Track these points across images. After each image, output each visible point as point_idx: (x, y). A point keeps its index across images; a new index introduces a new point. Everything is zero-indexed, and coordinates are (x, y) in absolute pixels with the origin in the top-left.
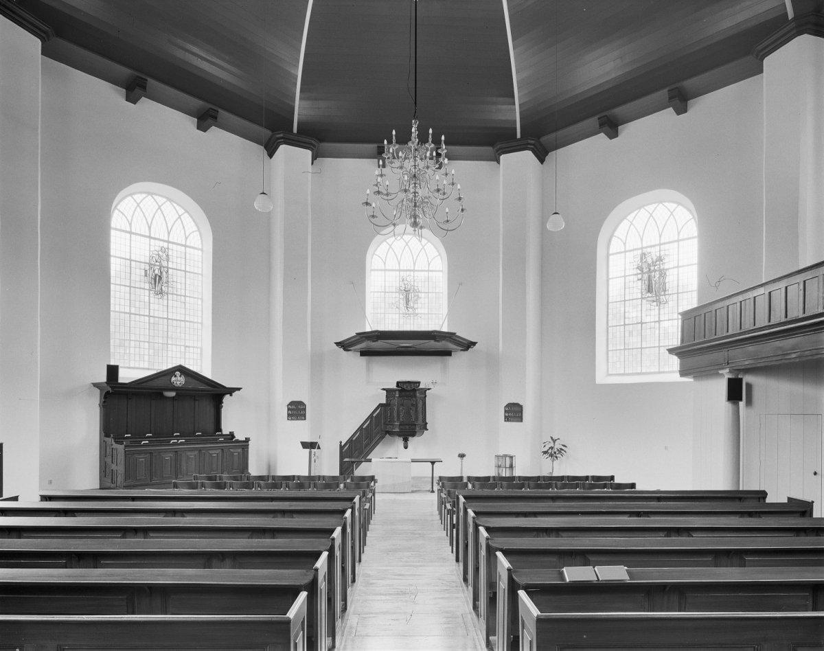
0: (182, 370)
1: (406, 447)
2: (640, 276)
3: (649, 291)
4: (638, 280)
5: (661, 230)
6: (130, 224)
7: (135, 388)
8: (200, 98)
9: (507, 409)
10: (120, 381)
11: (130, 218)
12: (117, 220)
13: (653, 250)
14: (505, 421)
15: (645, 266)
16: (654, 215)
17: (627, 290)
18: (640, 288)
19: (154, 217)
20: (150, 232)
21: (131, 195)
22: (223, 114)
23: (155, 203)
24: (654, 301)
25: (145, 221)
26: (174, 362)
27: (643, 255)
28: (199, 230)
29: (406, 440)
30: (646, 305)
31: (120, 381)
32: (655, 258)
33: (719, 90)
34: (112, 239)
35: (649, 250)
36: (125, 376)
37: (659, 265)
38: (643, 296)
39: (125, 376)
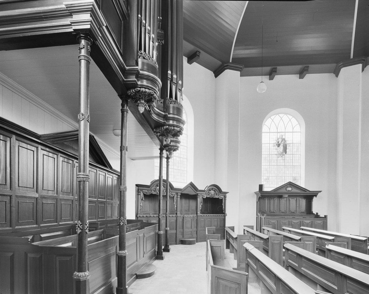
0: (291, 184)
5: (286, 126)
7: (273, 193)
8: (299, 64)
11: (269, 127)
12: (265, 129)
20: (277, 130)
21: (270, 117)
22: (311, 66)
23: (288, 118)
26: (280, 184)
28: (299, 124)
33: (359, 257)
34: (263, 137)
36: (265, 189)
39: (265, 189)
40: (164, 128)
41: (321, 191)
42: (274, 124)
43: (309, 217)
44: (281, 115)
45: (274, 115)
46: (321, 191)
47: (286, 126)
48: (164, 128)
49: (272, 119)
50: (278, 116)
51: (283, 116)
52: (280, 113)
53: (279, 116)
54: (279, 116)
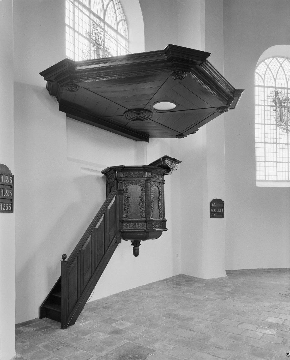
1: (136, 253)
2: (275, 108)
3: (281, 121)
4: (274, 111)
5: (275, 76)
6: (264, 81)
9: (213, 205)
10: (257, 186)
11: (263, 77)
13: (283, 91)
14: (211, 217)
15: (278, 101)
16: (283, 65)
17: (266, 116)
18: (275, 117)
19: (265, 73)
21: (263, 61)
24: (284, 129)
25: (260, 78)
27: (277, 93)
29: (136, 244)
30: (279, 130)
31: (257, 186)
32: (284, 98)
35: (280, 90)
37: (287, 103)
38: (278, 124)
40: (123, 178)
41: (182, 162)
42: (270, 72)
43: (104, 74)
44: (281, 60)
45: (269, 58)
46: (182, 162)
47: (275, 76)
48: (123, 178)
49: (266, 64)
50: (276, 61)
51: (282, 61)
52: (281, 57)
53: (278, 61)
54: (278, 61)
